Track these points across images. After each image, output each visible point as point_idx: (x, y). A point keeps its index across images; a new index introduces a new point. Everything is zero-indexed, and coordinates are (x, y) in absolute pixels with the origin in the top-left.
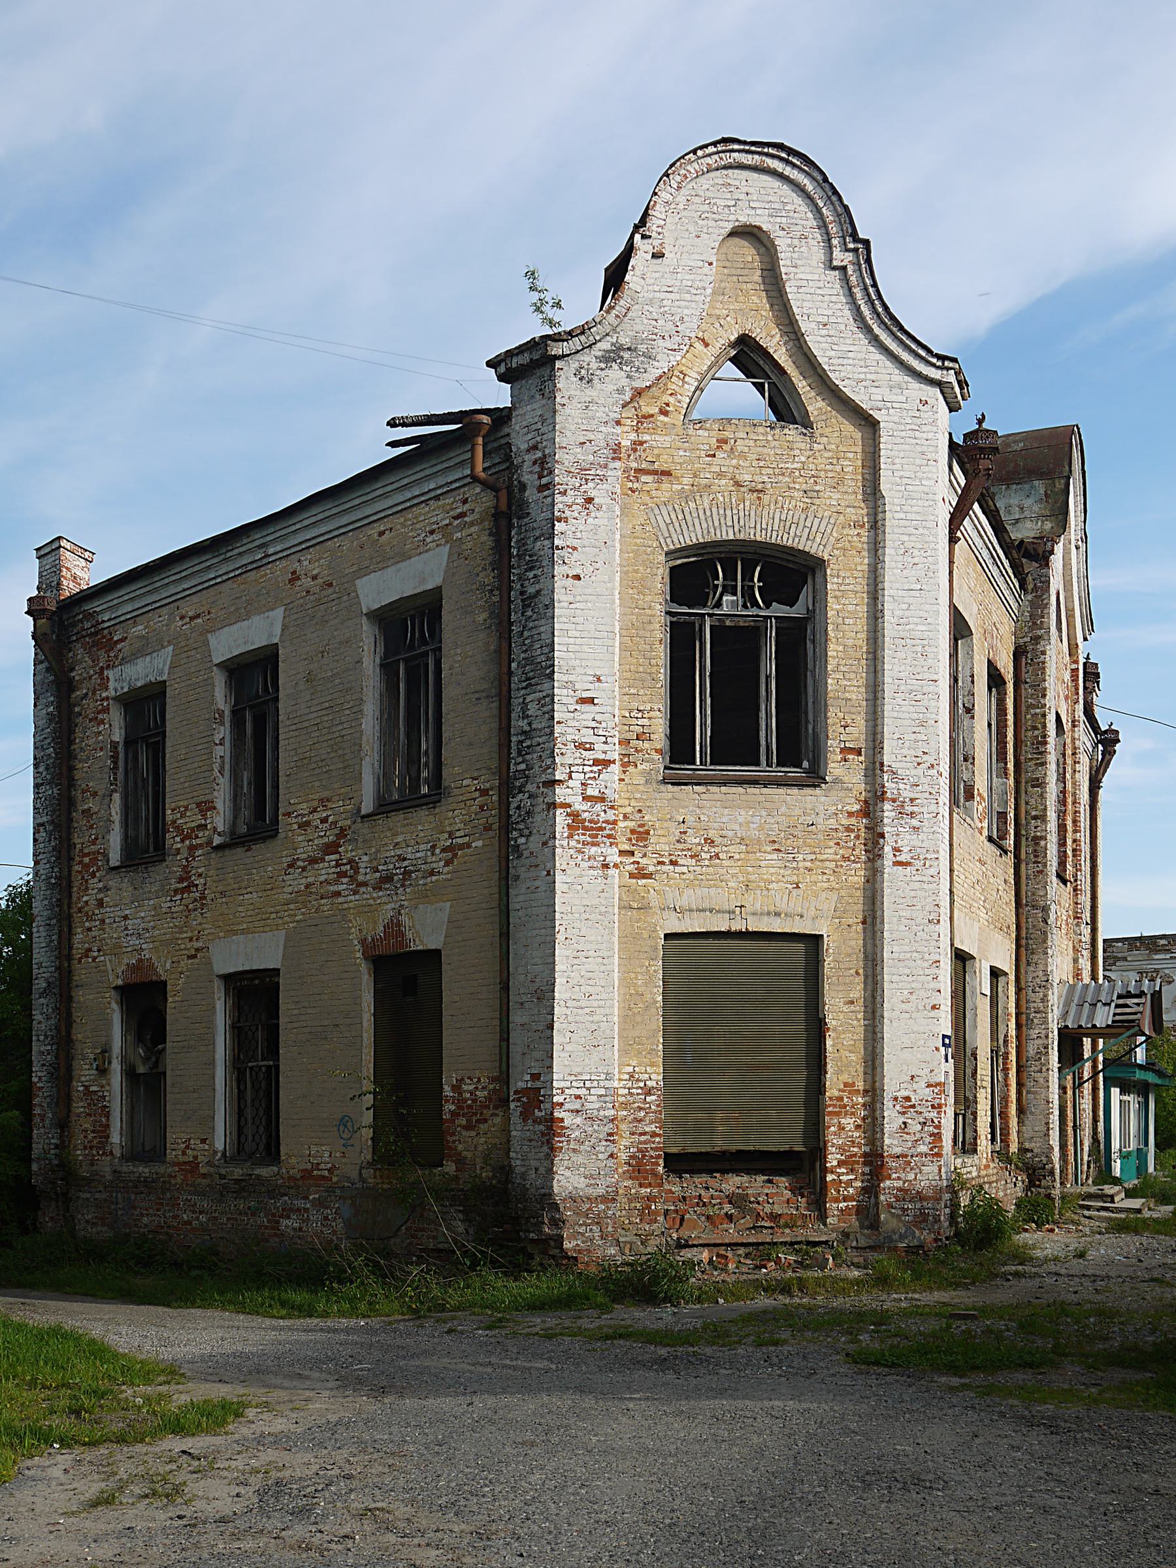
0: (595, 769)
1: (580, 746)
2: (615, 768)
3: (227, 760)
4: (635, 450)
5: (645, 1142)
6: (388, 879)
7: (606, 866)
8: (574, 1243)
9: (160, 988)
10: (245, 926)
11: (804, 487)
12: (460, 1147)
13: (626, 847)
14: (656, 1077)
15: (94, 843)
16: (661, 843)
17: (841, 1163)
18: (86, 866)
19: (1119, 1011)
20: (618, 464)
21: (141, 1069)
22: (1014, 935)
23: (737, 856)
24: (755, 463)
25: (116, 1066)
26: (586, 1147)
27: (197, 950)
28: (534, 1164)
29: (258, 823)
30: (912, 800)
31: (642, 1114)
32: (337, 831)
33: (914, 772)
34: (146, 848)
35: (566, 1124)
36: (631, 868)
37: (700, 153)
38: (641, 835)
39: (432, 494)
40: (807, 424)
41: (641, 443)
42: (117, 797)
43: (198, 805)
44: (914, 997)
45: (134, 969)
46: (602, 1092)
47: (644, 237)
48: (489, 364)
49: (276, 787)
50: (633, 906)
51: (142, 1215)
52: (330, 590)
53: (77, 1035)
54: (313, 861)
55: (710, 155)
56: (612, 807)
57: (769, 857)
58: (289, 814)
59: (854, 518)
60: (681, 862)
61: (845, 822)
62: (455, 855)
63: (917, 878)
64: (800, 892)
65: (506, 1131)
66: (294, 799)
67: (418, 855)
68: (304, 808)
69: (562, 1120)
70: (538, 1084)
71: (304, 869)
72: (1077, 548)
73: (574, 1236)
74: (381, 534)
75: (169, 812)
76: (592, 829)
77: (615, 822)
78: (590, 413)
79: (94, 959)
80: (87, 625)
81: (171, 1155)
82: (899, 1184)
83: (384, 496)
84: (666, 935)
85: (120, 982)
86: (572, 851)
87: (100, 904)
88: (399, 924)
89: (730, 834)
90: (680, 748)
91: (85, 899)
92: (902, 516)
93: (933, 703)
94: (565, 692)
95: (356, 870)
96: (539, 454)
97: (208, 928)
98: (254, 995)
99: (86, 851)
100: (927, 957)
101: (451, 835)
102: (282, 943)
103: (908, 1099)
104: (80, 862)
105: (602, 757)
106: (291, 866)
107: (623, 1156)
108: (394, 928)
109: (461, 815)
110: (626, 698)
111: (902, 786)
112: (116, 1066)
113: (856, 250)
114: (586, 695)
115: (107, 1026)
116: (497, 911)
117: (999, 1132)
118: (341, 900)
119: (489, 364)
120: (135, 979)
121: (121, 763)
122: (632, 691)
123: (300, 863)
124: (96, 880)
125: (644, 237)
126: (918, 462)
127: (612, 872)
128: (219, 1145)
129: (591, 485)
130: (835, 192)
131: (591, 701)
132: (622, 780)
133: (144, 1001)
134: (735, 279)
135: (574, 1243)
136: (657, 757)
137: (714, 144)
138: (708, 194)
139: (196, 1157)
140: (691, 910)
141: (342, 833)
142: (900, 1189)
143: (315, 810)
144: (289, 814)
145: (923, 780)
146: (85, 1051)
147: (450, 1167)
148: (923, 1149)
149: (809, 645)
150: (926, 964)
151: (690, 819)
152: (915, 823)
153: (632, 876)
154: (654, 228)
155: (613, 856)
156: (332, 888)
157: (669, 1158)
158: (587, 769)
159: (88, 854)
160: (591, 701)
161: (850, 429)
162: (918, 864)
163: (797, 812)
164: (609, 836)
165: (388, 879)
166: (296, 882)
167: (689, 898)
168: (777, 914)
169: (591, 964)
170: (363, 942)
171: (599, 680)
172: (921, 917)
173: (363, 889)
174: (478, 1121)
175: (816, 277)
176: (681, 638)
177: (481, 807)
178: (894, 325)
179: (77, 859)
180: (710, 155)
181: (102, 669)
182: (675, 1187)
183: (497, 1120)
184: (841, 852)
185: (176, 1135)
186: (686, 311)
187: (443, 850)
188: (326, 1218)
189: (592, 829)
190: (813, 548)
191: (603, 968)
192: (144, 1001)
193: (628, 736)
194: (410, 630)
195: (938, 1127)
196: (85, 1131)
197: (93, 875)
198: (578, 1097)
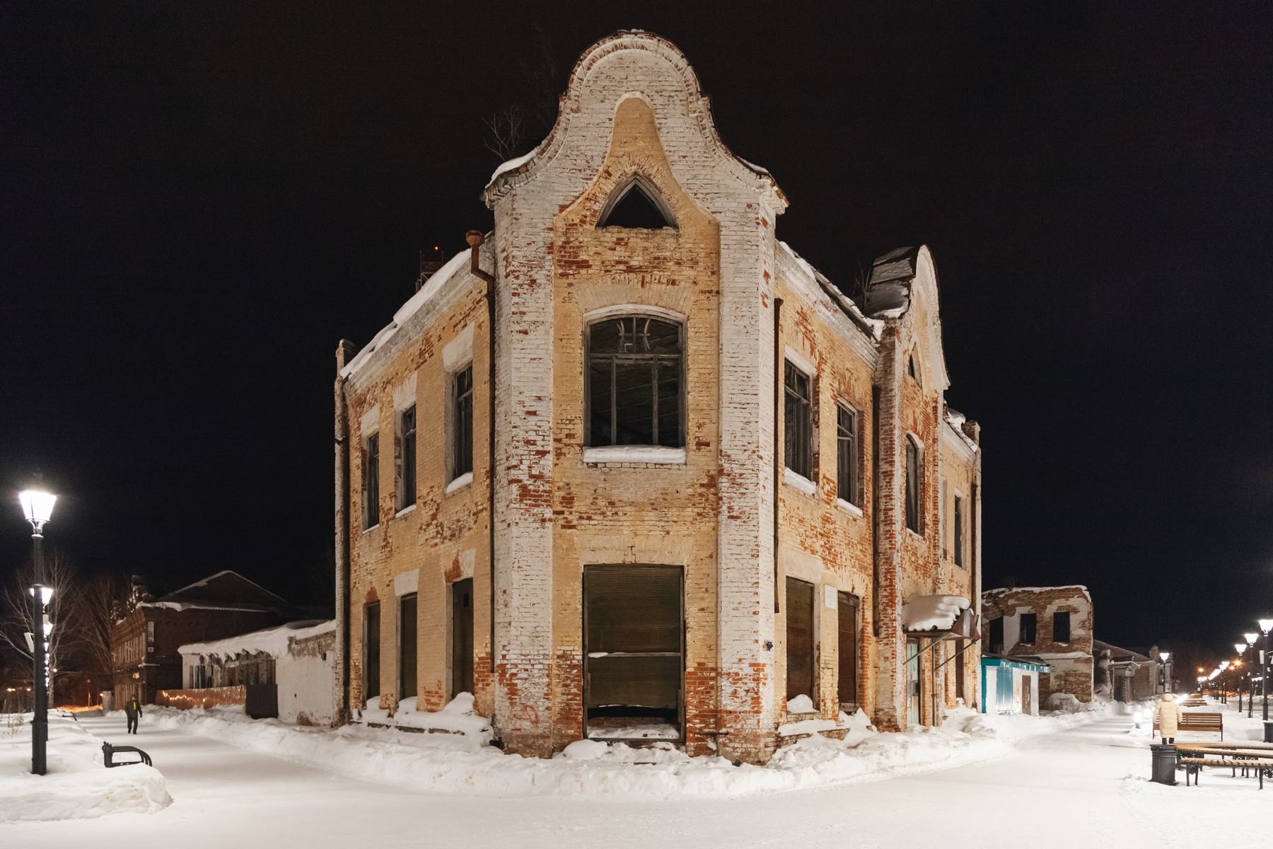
1: (528, 442)
2: (550, 458)
7: (543, 521)
13: (559, 508)
16: (580, 506)
17: (695, 716)
20: (550, 257)
22: (871, 572)
29: (410, 499)
36: (562, 522)
38: (568, 500)
50: (562, 553)
54: (428, 525)
66: (422, 489)
77: (550, 492)
89: (625, 499)
103: (737, 674)
114: (531, 409)
131: (534, 413)
148: (747, 708)
153: (563, 527)
155: (548, 513)
160: (534, 413)
162: (744, 517)
166: (422, 538)
167: (597, 542)
172: (745, 552)
190: (675, 316)
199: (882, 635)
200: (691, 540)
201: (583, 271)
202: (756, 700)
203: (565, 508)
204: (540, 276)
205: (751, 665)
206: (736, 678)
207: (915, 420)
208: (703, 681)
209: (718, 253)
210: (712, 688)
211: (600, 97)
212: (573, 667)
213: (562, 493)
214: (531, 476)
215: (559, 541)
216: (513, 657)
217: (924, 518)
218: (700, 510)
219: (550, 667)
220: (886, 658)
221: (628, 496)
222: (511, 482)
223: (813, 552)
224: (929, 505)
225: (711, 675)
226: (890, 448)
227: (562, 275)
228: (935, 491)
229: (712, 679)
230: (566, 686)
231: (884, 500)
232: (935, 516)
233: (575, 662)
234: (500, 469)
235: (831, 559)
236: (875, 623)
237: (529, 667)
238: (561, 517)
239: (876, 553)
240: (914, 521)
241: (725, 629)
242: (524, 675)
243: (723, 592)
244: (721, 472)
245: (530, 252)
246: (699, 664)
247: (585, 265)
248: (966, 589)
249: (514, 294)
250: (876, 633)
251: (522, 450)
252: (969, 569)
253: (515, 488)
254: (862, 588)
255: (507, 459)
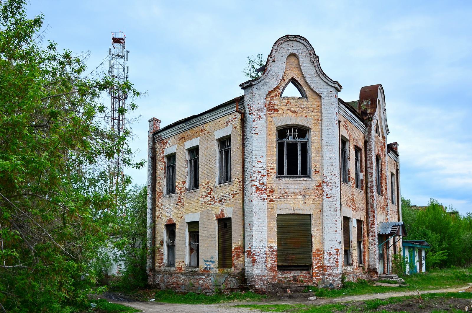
0: (261, 177)
1: (259, 172)
3: (188, 172)
4: (270, 105)
5: (273, 263)
6: (221, 201)
7: (264, 199)
8: (258, 286)
9: (174, 225)
10: (192, 211)
11: (306, 112)
12: (235, 264)
13: (269, 195)
14: (275, 247)
15: (160, 190)
16: (276, 194)
17: (316, 268)
18: (159, 196)
19: (392, 230)
20: (265, 108)
21: (170, 245)
22: (366, 211)
23: (292, 196)
24: (295, 106)
25: (165, 244)
26: (260, 264)
27: (182, 216)
28: (250, 268)
29: (195, 184)
30: (330, 183)
31: (272, 256)
32: (211, 189)
33: (331, 176)
34: (171, 190)
35: (256, 258)
37: (282, 38)
38: (272, 192)
39: (229, 113)
40: (306, 97)
41: (271, 103)
42: (165, 179)
43: (182, 182)
44: (331, 229)
45: (169, 220)
46: (264, 251)
47: (270, 57)
48: (240, 86)
49: (198, 178)
50: (270, 209)
51: (170, 280)
52: (209, 134)
53: (157, 237)
54: (206, 196)
55: (284, 39)
56: (265, 186)
57: (299, 196)
58: (201, 185)
59: (317, 118)
60: (280, 198)
61: (316, 188)
62: (234, 196)
63: (332, 201)
64: (306, 204)
65: (244, 260)
66: (202, 181)
67: (227, 195)
68: (204, 184)
69: (255, 258)
70: (250, 249)
71: (204, 198)
72: (384, 113)
73: (258, 285)
74: (219, 121)
75: (176, 183)
76: (261, 191)
77: (266, 189)
78: (260, 97)
79: (160, 218)
80: (159, 138)
81: (176, 266)
82: (329, 273)
83: (220, 113)
84: (277, 215)
85: (166, 224)
86: (257, 196)
87: (162, 205)
88: (223, 212)
89: (291, 191)
90: (280, 172)
91: (159, 203)
92: (327, 117)
93: (334, 160)
94: (255, 160)
95: (214, 198)
96: (249, 106)
97: (184, 211)
98: (193, 228)
99: (159, 192)
100: (334, 219)
101: (233, 191)
102: (199, 215)
103: (330, 253)
104: (157, 195)
105: (263, 174)
106: (201, 197)
107: (268, 266)
108: (222, 212)
109: (235, 186)
110: (268, 161)
111: (328, 180)
112: (165, 244)
113: (316, 58)
115: (162, 234)
116: (242, 209)
117: (361, 260)
118: (211, 205)
119: (240, 86)
120: (169, 223)
121: (166, 171)
122: (270, 159)
123: (203, 197)
124: (161, 199)
125: (270, 57)
126: (330, 105)
127: (265, 200)
128: (187, 263)
129: (260, 113)
130: (311, 46)
131: (260, 162)
132: (267, 179)
133: (171, 228)
134: (290, 65)
135: (258, 286)
136: (275, 174)
137: (285, 36)
138: (285, 47)
139: (181, 266)
140: (283, 209)
141: (212, 190)
142: (329, 274)
143: (206, 184)
144: (201, 185)
145: (332, 178)
146: (158, 241)
147: (233, 269)
148: (334, 264)
149: (308, 147)
150: (334, 221)
151: (282, 188)
152: (331, 188)
153: (270, 201)
154: (273, 55)
155: (265, 197)
156: (210, 203)
157: (278, 266)
158: (260, 177)
159: (159, 193)
160: (260, 162)
161: (315, 97)
163: (305, 186)
164: (265, 192)
165: (221, 201)
166: (202, 201)
167: (282, 206)
168: (301, 210)
169: (261, 221)
170: (216, 215)
171: (262, 157)
172: (333, 210)
173: (216, 203)
174: (239, 258)
175: (307, 64)
176: (280, 146)
177: (239, 185)
178: (324, 74)
179: (157, 194)
180: (284, 39)
181: (162, 149)
182: (280, 275)
183: (242, 257)
184: (315, 195)
185: (177, 260)
186: (280, 73)
187: (232, 195)
188: (208, 281)
189: (261, 191)
191: (263, 222)
192: (171, 228)
193: (269, 169)
194: (225, 142)
195: (337, 259)
196: (158, 259)
197: (160, 198)
198: (258, 252)
199: (370, 236)
200: (314, 205)
201: (276, 112)
202: (337, 262)
203: (269, 193)
204: (262, 115)
205: (335, 249)
206: (330, 254)
207: (378, 150)
208: (318, 255)
209: (321, 107)
210: (321, 258)
211: (281, 55)
212: (274, 251)
213: (270, 189)
214: (260, 184)
215: (268, 206)
216: (254, 248)
217: (382, 187)
218: (316, 195)
219: (266, 251)
220: (372, 245)
221: (292, 190)
222: (252, 185)
223: (350, 206)
224: (384, 182)
225: (321, 254)
226: (371, 163)
227: (269, 114)
228: (385, 176)
229: (321, 254)
230: (271, 258)
231: (369, 183)
232: (386, 186)
233: (274, 249)
234: (248, 182)
235: (355, 208)
236: (368, 231)
237: (259, 251)
238: (269, 197)
239: (367, 203)
240: (380, 192)
241: (326, 237)
242: (258, 254)
243: (325, 224)
244: (323, 182)
245: (259, 107)
246: (317, 249)
247: (277, 110)
248: (396, 213)
249: (253, 121)
250: (368, 235)
251: (257, 174)
252: (397, 205)
253: (254, 188)
254: (363, 219)
255: (251, 178)
